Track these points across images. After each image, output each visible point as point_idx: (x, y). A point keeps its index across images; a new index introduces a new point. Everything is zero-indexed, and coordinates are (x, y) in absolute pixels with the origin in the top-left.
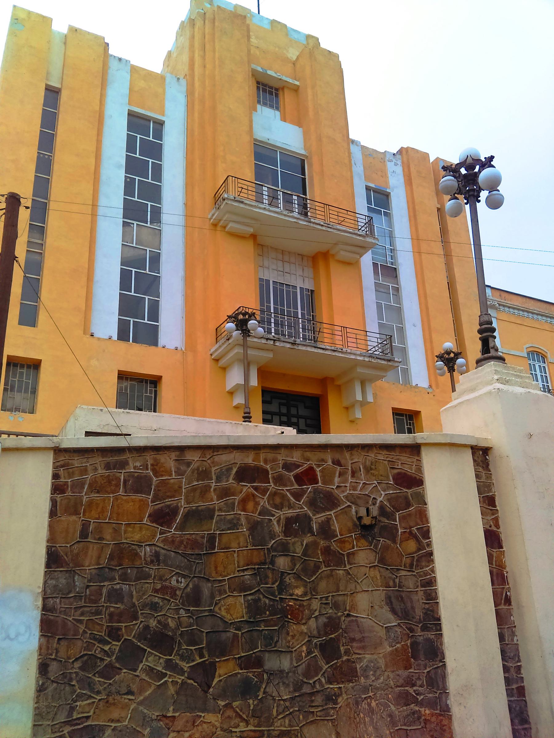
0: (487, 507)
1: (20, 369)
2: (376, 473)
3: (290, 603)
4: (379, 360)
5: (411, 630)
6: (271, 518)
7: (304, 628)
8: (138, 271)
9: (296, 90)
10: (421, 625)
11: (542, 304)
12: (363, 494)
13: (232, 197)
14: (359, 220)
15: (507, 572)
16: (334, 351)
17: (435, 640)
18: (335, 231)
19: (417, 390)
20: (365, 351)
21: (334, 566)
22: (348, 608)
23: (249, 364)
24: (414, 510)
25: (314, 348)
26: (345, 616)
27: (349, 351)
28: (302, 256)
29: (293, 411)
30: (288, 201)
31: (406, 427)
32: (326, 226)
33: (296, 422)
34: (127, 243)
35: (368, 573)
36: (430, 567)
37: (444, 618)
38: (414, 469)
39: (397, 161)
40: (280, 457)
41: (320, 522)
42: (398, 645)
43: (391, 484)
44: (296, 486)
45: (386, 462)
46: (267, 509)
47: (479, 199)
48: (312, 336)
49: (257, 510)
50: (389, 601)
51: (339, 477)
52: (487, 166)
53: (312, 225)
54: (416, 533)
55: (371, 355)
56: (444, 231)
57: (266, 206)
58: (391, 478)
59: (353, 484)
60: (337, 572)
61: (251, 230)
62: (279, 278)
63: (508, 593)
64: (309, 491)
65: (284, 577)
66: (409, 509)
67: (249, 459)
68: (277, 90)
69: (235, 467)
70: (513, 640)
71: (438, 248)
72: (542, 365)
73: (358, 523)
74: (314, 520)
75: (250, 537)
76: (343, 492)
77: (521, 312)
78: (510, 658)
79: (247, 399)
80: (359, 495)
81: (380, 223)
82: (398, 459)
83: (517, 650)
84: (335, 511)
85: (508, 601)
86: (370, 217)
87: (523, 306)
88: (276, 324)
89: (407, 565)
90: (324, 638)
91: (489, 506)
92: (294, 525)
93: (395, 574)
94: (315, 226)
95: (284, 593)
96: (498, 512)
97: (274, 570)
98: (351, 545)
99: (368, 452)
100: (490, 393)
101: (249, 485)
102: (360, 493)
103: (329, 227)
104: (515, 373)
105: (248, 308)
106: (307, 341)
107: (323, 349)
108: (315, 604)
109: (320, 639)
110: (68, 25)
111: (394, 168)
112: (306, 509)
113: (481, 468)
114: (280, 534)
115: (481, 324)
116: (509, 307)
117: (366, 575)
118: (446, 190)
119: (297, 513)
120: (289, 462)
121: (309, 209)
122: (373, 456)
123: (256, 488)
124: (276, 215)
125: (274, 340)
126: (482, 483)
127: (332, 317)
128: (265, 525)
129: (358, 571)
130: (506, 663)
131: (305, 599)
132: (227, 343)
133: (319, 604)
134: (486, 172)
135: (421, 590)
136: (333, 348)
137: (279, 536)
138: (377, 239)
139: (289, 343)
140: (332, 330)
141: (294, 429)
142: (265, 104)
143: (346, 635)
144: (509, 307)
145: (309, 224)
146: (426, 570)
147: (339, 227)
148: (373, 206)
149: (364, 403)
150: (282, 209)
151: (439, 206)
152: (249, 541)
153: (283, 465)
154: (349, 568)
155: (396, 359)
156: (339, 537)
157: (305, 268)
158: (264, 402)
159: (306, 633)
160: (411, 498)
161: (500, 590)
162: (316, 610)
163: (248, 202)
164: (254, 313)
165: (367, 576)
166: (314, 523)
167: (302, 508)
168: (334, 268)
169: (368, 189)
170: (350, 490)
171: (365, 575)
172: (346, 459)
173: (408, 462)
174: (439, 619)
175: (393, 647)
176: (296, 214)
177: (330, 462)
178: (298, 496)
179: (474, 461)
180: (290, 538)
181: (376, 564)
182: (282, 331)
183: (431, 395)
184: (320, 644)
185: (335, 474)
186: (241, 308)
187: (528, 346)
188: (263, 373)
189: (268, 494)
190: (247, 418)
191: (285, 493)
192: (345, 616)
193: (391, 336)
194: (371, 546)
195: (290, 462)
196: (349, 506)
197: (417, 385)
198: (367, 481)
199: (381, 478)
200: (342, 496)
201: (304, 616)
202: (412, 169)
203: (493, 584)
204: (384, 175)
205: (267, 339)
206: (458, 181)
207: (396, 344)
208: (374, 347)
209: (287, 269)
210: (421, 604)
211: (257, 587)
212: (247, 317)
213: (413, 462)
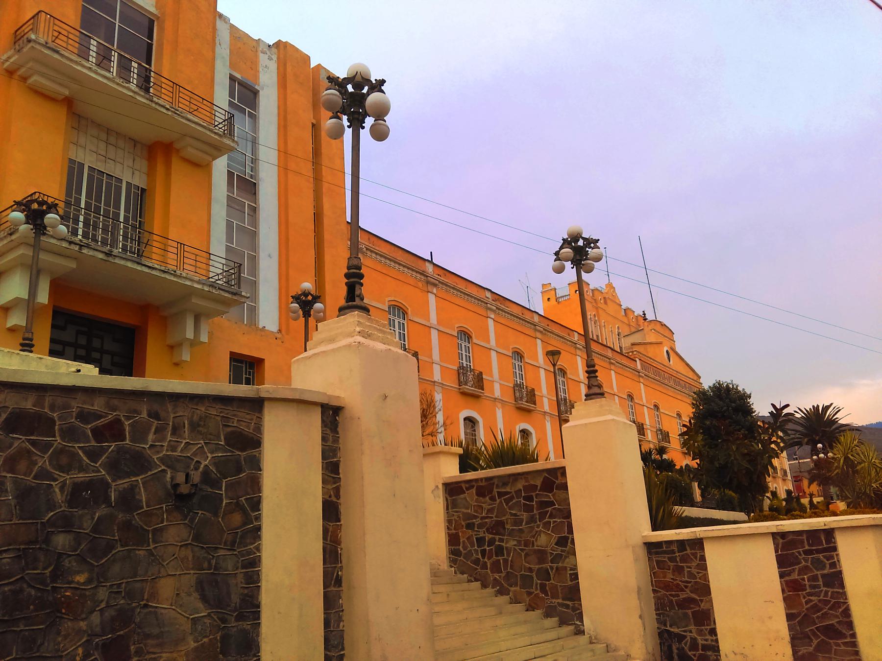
0: (329, 474)
2: (203, 430)
3: (67, 594)
4: (221, 292)
5: (224, 621)
6: (52, 483)
7: (83, 624)
10: (236, 614)
11: (410, 256)
12: (184, 456)
13: (42, 41)
14: (217, 114)
15: (341, 549)
16: (164, 272)
17: (251, 630)
18: (184, 121)
19: (263, 333)
20: (205, 278)
21: (134, 545)
22: (146, 597)
23: (39, 272)
24: (245, 476)
25: (136, 265)
26: (141, 608)
27: (184, 275)
28: (135, 142)
29: (96, 343)
30: (125, 67)
31: (244, 376)
32: (172, 111)
33: (99, 358)
35: (177, 553)
36: (256, 544)
37: (265, 604)
38: (252, 428)
39: (272, 55)
40: (74, 404)
41: (121, 489)
42: (205, 640)
43: (221, 445)
44: (94, 443)
45: (219, 419)
46: (48, 471)
47: (363, 125)
48: (135, 248)
49: (32, 471)
50: (200, 586)
51: (155, 434)
52: (376, 90)
53: (154, 105)
54: (244, 504)
55: (213, 284)
56: (317, 152)
57: (92, 65)
58: (222, 438)
59: (172, 443)
60: (137, 552)
61: (67, 93)
62: (99, 164)
63: (340, 573)
64: (110, 450)
65: (61, 560)
66: (239, 475)
67: (28, 404)
69: (5, 413)
70: (338, 626)
71: (307, 169)
72: (401, 322)
73: (172, 492)
74: (113, 487)
75: (17, 507)
76: (158, 452)
77: (388, 261)
78: (333, 647)
79: (30, 320)
80: (179, 457)
81: (242, 125)
82: (234, 415)
83: (342, 637)
84: (143, 476)
85: (339, 582)
86: (231, 114)
87: (391, 255)
88: (86, 223)
89: (228, 543)
90: (110, 636)
91: (331, 473)
92: (84, 494)
93: (212, 554)
94: (157, 107)
95: (59, 581)
96: (340, 481)
97: (48, 550)
98: (160, 519)
99: (197, 405)
100: (349, 346)
101: (24, 438)
102: (180, 454)
103: (176, 113)
104: (378, 327)
105: (48, 196)
106: (128, 254)
107: (149, 267)
108: (103, 594)
109: (103, 638)
111: (268, 62)
112: (104, 473)
113: (328, 429)
114: (63, 505)
115: (349, 268)
116: (376, 254)
117: (175, 556)
118: (329, 105)
119: (89, 478)
120: (86, 410)
121: (152, 84)
122: (203, 409)
123: (33, 443)
124: (105, 81)
125: (81, 246)
126: (327, 448)
127: (166, 226)
128: (42, 492)
129: (165, 552)
130: (328, 653)
131: (89, 587)
132: (9, 239)
133: (108, 593)
134: (374, 97)
135: (241, 573)
136: (163, 268)
137: (61, 507)
138: (237, 142)
140: (165, 245)
141: (95, 367)
143: (139, 631)
144: (376, 254)
145: (150, 103)
146: (250, 549)
147: (190, 116)
148: (236, 102)
149: (194, 343)
150: (115, 74)
151: (314, 122)
152: (14, 513)
153: (77, 415)
154: (153, 548)
155: (243, 294)
156: (145, 509)
157: (136, 158)
158: (53, 326)
159: (85, 631)
160: (244, 463)
161: (330, 569)
162: (102, 601)
163: (66, 54)
164: (57, 205)
165: (176, 558)
166: (113, 491)
167: (99, 471)
168: (177, 165)
169: (232, 79)
170: (167, 450)
171: (174, 555)
172: (168, 412)
173: (246, 419)
174: (258, 606)
175: (199, 642)
176: (133, 87)
177: (144, 415)
178: (94, 455)
179: (323, 421)
180: (77, 510)
181: (190, 542)
182: (94, 236)
183: (279, 342)
184: (102, 644)
185: (150, 429)
186: (37, 194)
188: (56, 287)
189: (51, 451)
190: (27, 346)
191: (75, 451)
192: (141, 608)
193: (241, 265)
194: (185, 519)
195: (89, 410)
196: (163, 471)
198: (192, 440)
199: (209, 436)
200: (155, 457)
201: (85, 610)
202: (289, 69)
203: (324, 563)
204: (254, 65)
205: (71, 243)
206: (343, 99)
207: (245, 275)
208: (218, 275)
210: (239, 589)
211: (19, 574)
212: (44, 207)
213: (252, 420)
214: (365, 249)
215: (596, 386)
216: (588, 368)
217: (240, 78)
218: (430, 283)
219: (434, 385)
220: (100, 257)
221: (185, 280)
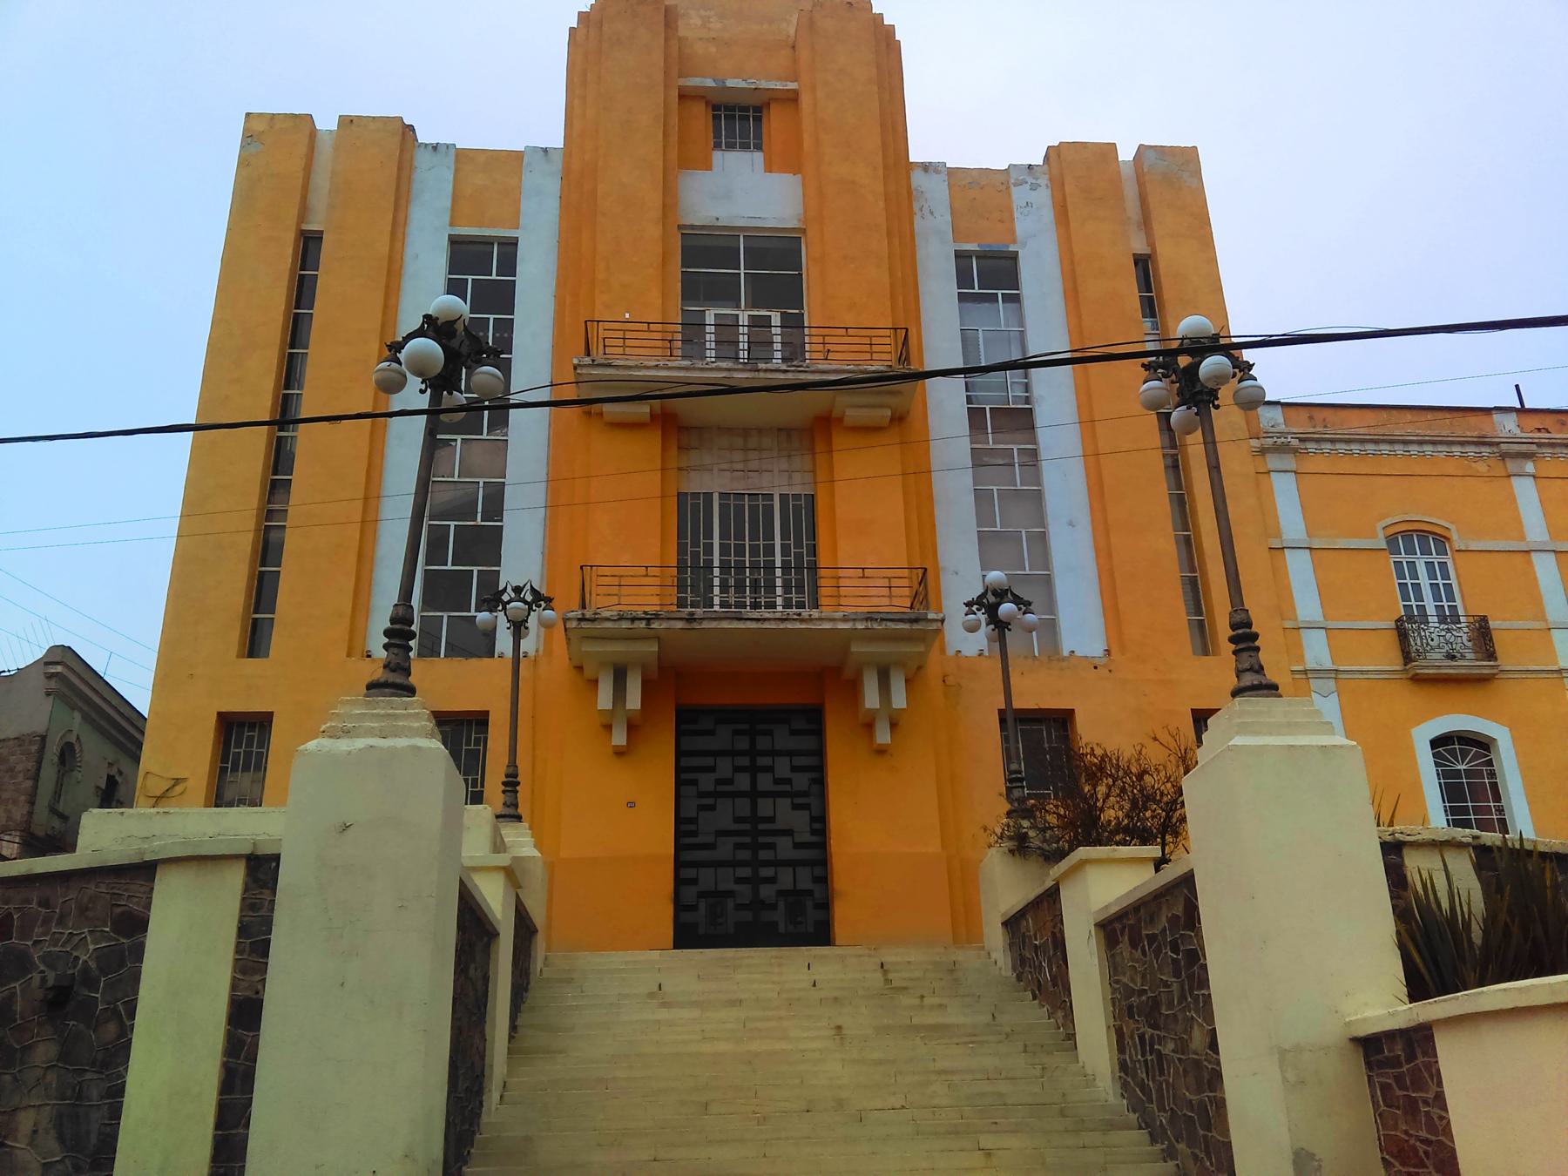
4: (889, 624)
9: (792, 98)
32: (793, 371)
34: (443, 477)
43: (107, 932)
59: (57, 936)
77: (1370, 447)
82: (126, 890)
115: (393, 621)
125: (649, 619)
142: (730, 146)
168: (839, 440)
183: (1103, 672)
187: (1389, 521)
197: (1073, 652)
209: (754, 465)
214: (1295, 443)
215: (1248, 670)
216: (1233, 631)
217: (978, 249)
218: (1509, 455)
219: (1308, 678)
220: (680, 627)
221: (820, 622)
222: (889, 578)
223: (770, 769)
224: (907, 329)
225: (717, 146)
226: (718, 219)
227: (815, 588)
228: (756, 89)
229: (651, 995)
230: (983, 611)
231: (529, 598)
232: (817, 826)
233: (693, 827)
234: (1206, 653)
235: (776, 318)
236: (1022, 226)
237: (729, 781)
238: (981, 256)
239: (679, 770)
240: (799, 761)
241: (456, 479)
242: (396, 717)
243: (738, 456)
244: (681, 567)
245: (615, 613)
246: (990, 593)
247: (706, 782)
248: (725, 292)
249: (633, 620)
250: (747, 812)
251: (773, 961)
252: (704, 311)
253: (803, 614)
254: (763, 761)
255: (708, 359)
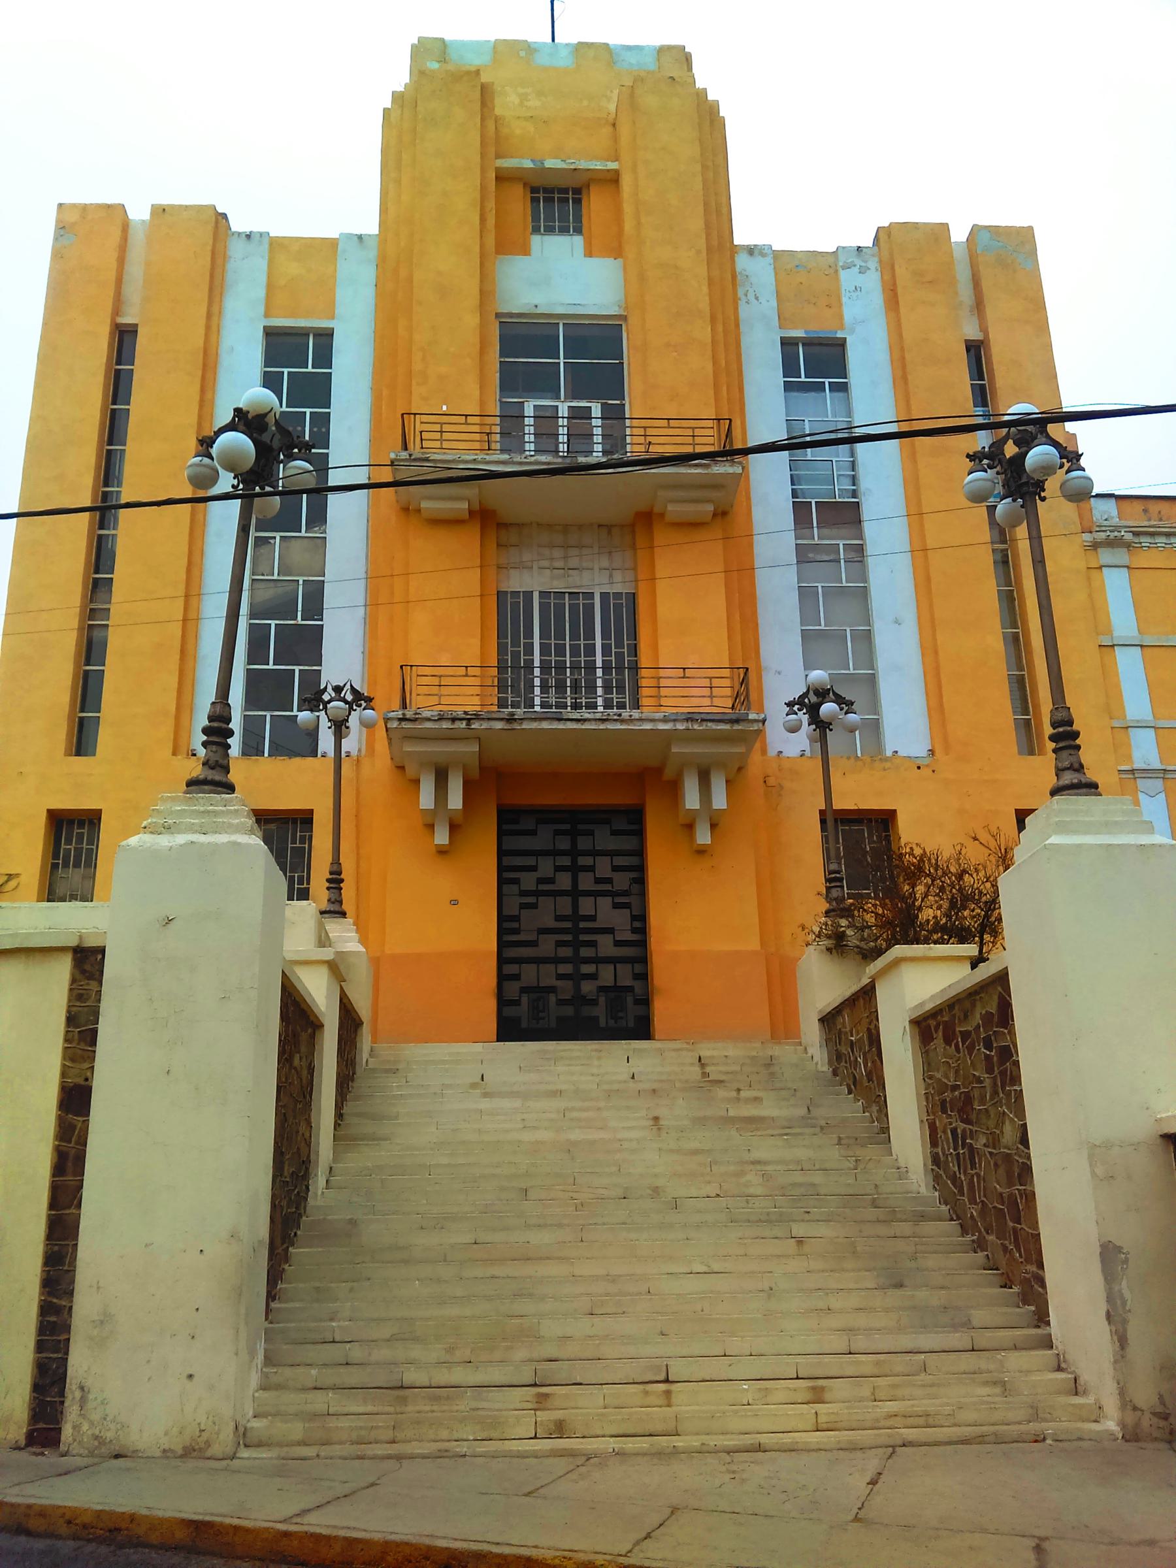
1: (77, 829)
4: (709, 724)
8: (282, 622)
9: (613, 179)
28: (607, 528)
34: (263, 575)
39: (866, 262)
57: (476, 455)
68: (578, 191)
110: (150, 206)
111: (860, 280)
125: (469, 720)
139: (502, 719)
142: (550, 230)
183: (926, 772)
197: (896, 752)
202: (900, 271)
204: (833, 300)
209: (574, 562)
222: (711, 678)
223: (591, 869)
224: (730, 420)
225: (536, 230)
226: (536, 306)
227: (636, 688)
228: (575, 169)
229: (474, 1086)
230: (805, 711)
231: (349, 697)
232: (637, 924)
233: (515, 925)
234: (1031, 753)
235: (596, 409)
236: (851, 310)
237: (551, 881)
238: (808, 343)
239: (501, 869)
240: (620, 861)
241: (276, 577)
242: (216, 814)
243: (558, 553)
244: (502, 668)
245: (436, 713)
246: (811, 693)
247: (528, 881)
248: (544, 383)
249: (454, 720)
250: (568, 911)
251: (594, 1053)
252: (523, 402)
253: (623, 714)
254: (583, 861)
255: (527, 453)
